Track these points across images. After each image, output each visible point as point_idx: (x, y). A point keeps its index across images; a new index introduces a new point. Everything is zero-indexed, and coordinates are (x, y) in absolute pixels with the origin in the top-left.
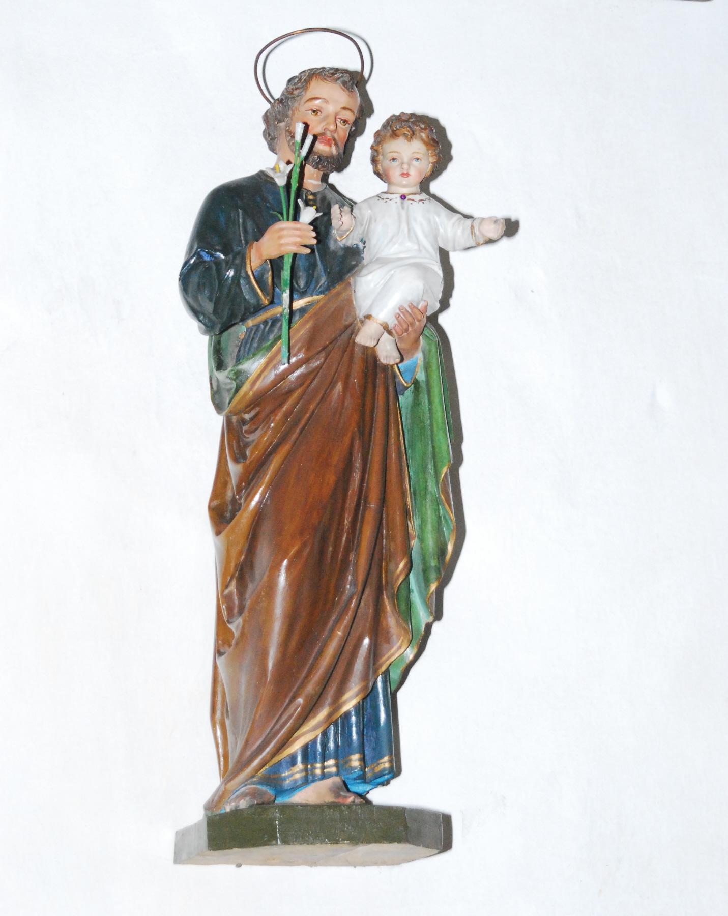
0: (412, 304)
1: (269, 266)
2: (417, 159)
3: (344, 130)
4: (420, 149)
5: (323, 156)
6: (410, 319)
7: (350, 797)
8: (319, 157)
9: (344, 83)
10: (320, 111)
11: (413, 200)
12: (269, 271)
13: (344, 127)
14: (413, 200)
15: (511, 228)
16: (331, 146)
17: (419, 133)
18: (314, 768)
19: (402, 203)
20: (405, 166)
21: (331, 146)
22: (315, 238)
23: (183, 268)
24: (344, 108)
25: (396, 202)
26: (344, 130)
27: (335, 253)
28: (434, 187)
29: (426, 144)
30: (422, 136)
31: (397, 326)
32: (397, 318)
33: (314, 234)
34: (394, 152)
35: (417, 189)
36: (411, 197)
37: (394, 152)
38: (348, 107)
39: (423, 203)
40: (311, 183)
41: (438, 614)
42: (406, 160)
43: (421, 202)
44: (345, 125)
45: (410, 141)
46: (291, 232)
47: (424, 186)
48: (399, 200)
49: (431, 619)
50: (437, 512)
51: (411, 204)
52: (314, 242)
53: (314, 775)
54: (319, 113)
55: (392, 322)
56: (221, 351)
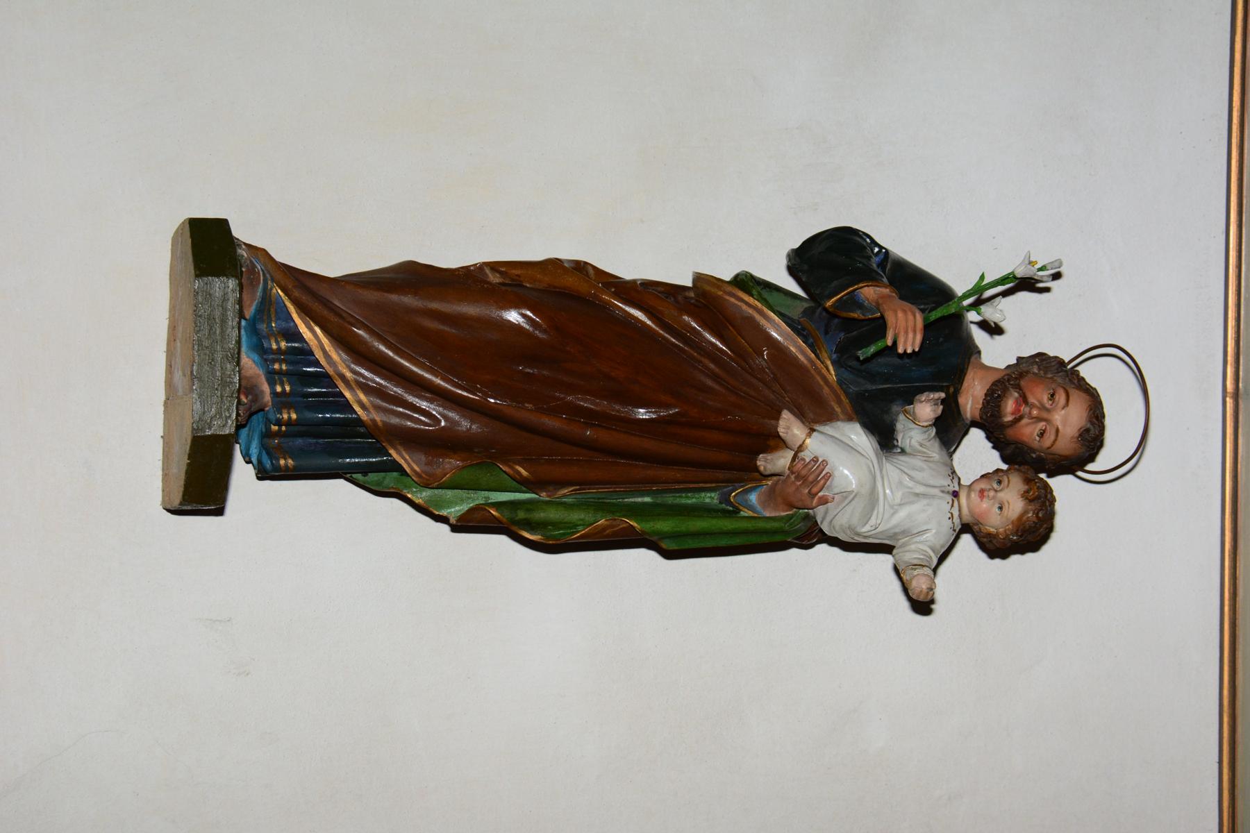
0: (830, 476)
1: (870, 317)
2: (1001, 508)
3: (1032, 433)
4: (1013, 510)
5: (1000, 402)
6: (811, 478)
7: (247, 398)
8: (999, 396)
9: (1087, 430)
10: (1053, 403)
11: (952, 506)
12: (863, 315)
13: (1036, 434)
14: (952, 506)
15: (922, 606)
16: (1012, 414)
17: (1032, 510)
18: (281, 362)
19: (948, 492)
20: (992, 493)
21: (1012, 414)
22: (905, 351)
23: (862, 232)
24: (1057, 431)
25: (949, 485)
26: (1032, 433)
27: (888, 412)
28: (967, 539)
29: (1020, 518)
30: (1028, 513)
31: (803, 462)
32: (813, 460)
33: (909, 351)
34: (1009, 481)
35: (967, 518)
36: (956, 503)
37: (1009, 481)
38: (1060, 435)
39: (949, 518)
40: (968, 401)
41: (462, 526)
42: (1001, 495)
43: (950, 515)
44: (1038, 436)
45: (1022, 497)
46: (911, 324)
47: (966, 528)
48: (951, 489)
49: (453, 521)
50: (581, 522)
51: (948, 503)
52: (900, 350)
53: (274, 361)
54: (1050, 402)
55: (807, 455)
56: (768, 289)
